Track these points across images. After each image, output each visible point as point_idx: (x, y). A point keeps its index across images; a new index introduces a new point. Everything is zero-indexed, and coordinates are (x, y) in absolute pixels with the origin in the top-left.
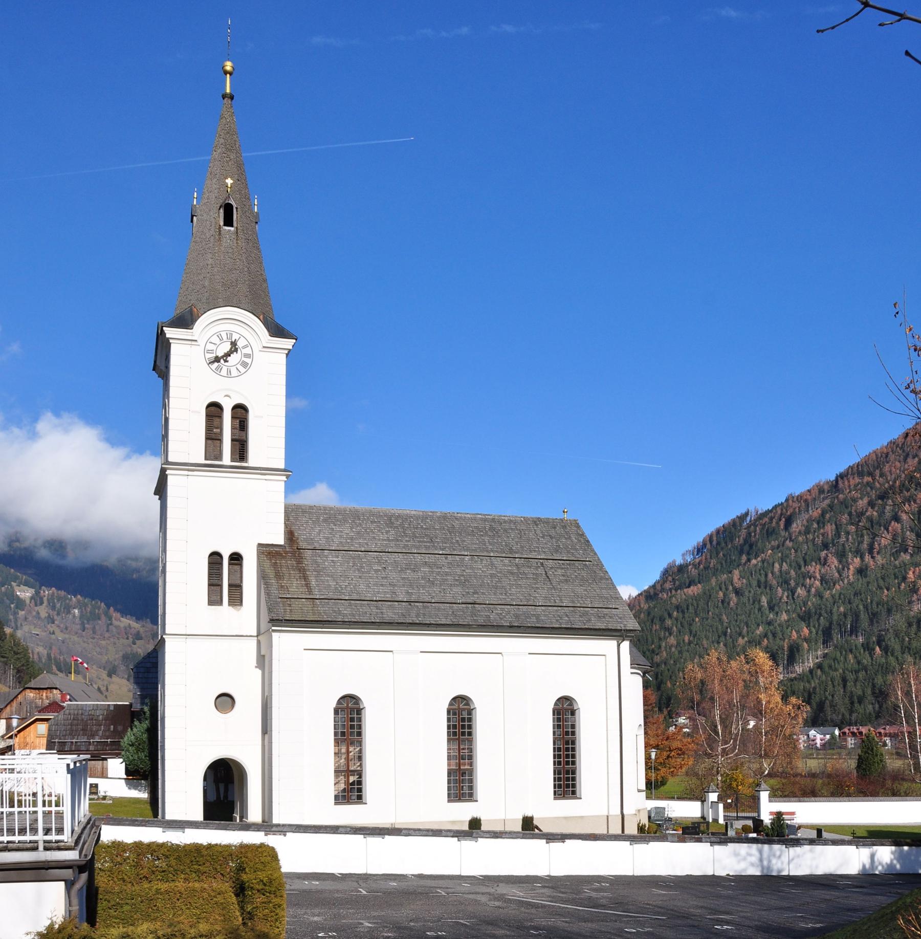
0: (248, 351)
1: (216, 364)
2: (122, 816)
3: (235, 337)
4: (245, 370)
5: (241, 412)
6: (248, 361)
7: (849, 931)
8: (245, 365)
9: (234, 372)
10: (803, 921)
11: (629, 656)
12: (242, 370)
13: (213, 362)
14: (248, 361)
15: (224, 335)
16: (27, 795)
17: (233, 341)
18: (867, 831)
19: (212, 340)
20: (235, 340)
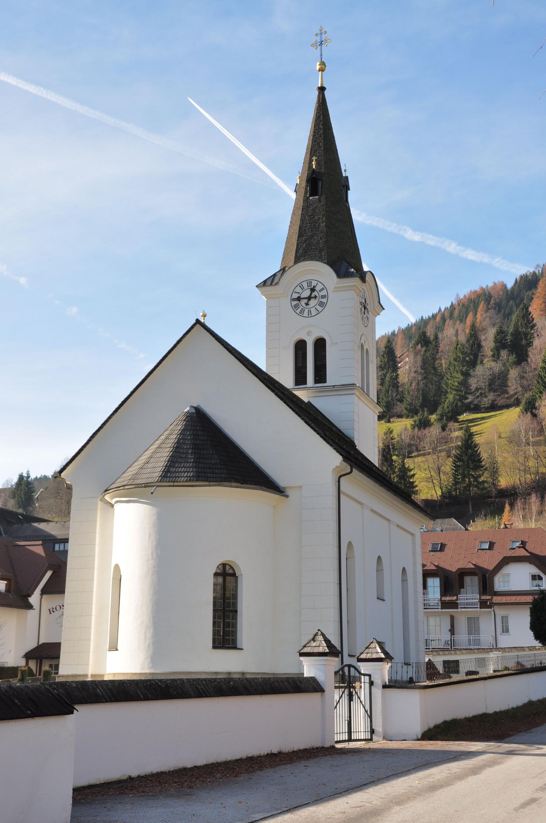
0: (324, 293)
1: (296, 302)
2: (259, 376)
3: (314, 283)
4: (323, 308)
5: (320, 344)
6: (324, 300)
7: (321, 239)
8: (322, 304)
9: (314, 312)
10: (324, 419)
11: (269, 170)
12: (320, 309)
13: (294, 300)
14: (324, 300)
15: (305, 285)
16: (388, 767)
17: (312, 287)
18: (235, 648)
19: (296, 290)
20: (314, 286)
